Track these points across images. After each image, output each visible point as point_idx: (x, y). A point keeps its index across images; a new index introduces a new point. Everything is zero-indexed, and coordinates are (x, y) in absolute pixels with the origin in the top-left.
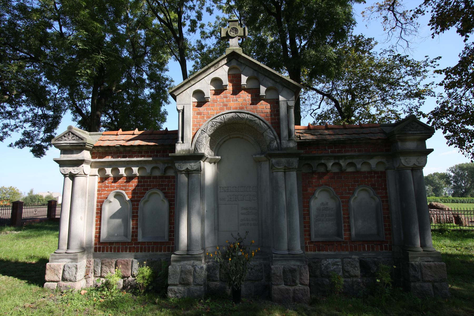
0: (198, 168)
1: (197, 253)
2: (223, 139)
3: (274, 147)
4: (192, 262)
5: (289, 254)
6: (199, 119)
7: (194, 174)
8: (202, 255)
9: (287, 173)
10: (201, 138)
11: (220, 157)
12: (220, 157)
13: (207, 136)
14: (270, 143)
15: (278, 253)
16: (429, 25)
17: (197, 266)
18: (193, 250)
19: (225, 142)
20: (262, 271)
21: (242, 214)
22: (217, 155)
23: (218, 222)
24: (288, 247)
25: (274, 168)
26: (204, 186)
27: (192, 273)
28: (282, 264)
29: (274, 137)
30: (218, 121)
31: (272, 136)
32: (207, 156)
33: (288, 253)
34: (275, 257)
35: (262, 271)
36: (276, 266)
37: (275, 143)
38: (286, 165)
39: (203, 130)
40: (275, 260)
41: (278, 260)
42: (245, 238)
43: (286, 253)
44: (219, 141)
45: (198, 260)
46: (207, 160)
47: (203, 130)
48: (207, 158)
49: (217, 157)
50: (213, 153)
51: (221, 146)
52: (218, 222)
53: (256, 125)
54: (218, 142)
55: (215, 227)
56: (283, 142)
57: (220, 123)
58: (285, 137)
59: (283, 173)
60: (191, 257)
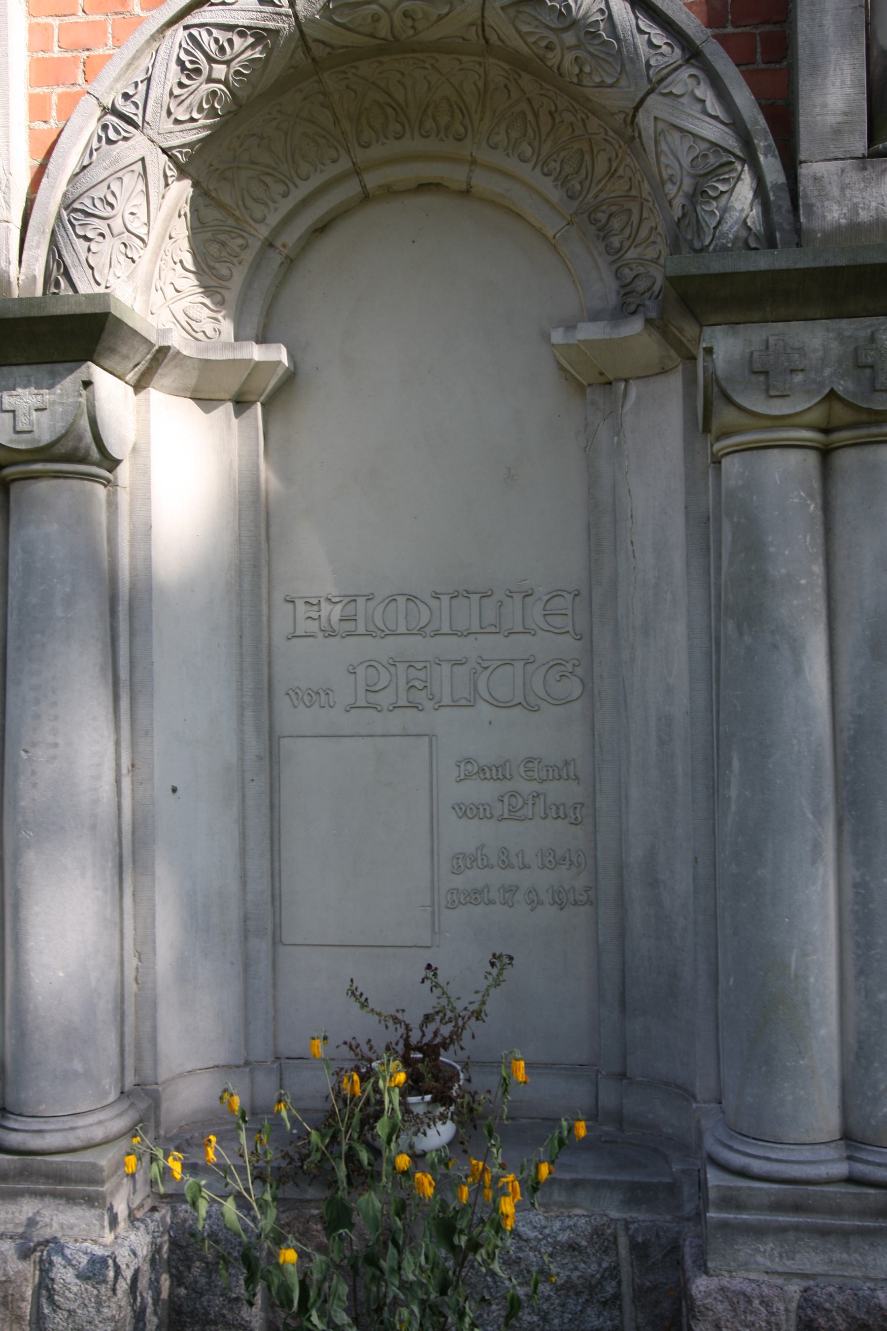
0: (70, 432)
1: (73, 1140)
2: (306, 202)
3: (731, 226)
4: (27, 1208)
5: (851, 1180)
6: (81, 17)
7: (44, 486)
8: (104, 1159)
9: (846, 459)
10: (97, 173)
11: (280, 354)
12: (280, 354)
13: (158, 163)
14: (698, 195)
15: (757, 1166)
16: (484, 1021)
17: (60, 1250)
18: (42, 1109)
19: (321, 229)
20: (617, 1296)
21: (464, 811)
22: (262, 339)
23: (275, 874)
24: (845, 1109)
25: (726, 416)
26: (150, 590)
27: (27, 1308)
28: (791, 1265)
29: (731, 142)
30: (242, 20)
31: (713, 131)
32: (165, 333)
33: (841, 1169)
34: (730, 1201)
35: (617, 1296)
36: (737, 1282)
37: (745, 191)
38: (843, 387)
39: (114, 111)
40: (724, 1225)
41: (758, 1232)
42: (478, 1015)
43: (822, 1171)
44: (274, 219)
45: (71, 1199)
46: (166, 376)
47: (114, 111)
48: (164, 351)
49: (256, 353)
50: (227, 328)
51: (290, 263)
52: (275, 874)
53: (569, 38)
54: (263, 232)
55: (245, 919)
56: (816, 179)
57: (260, 35)
58: (837, 132)
59: (811, 459)
60: (23, 1174)
